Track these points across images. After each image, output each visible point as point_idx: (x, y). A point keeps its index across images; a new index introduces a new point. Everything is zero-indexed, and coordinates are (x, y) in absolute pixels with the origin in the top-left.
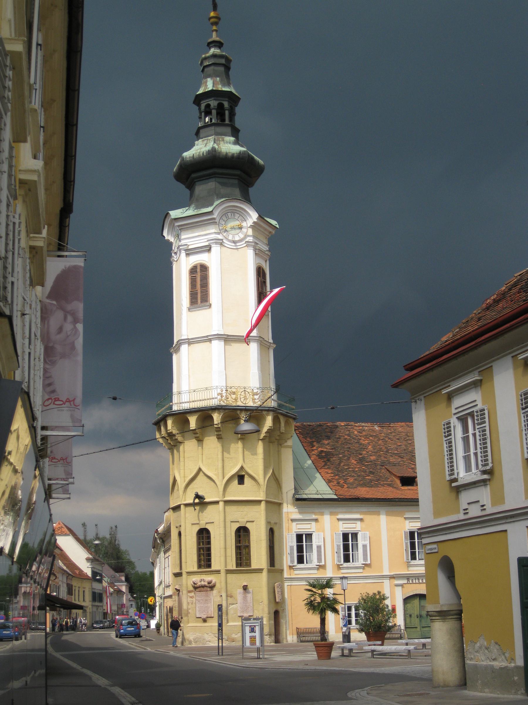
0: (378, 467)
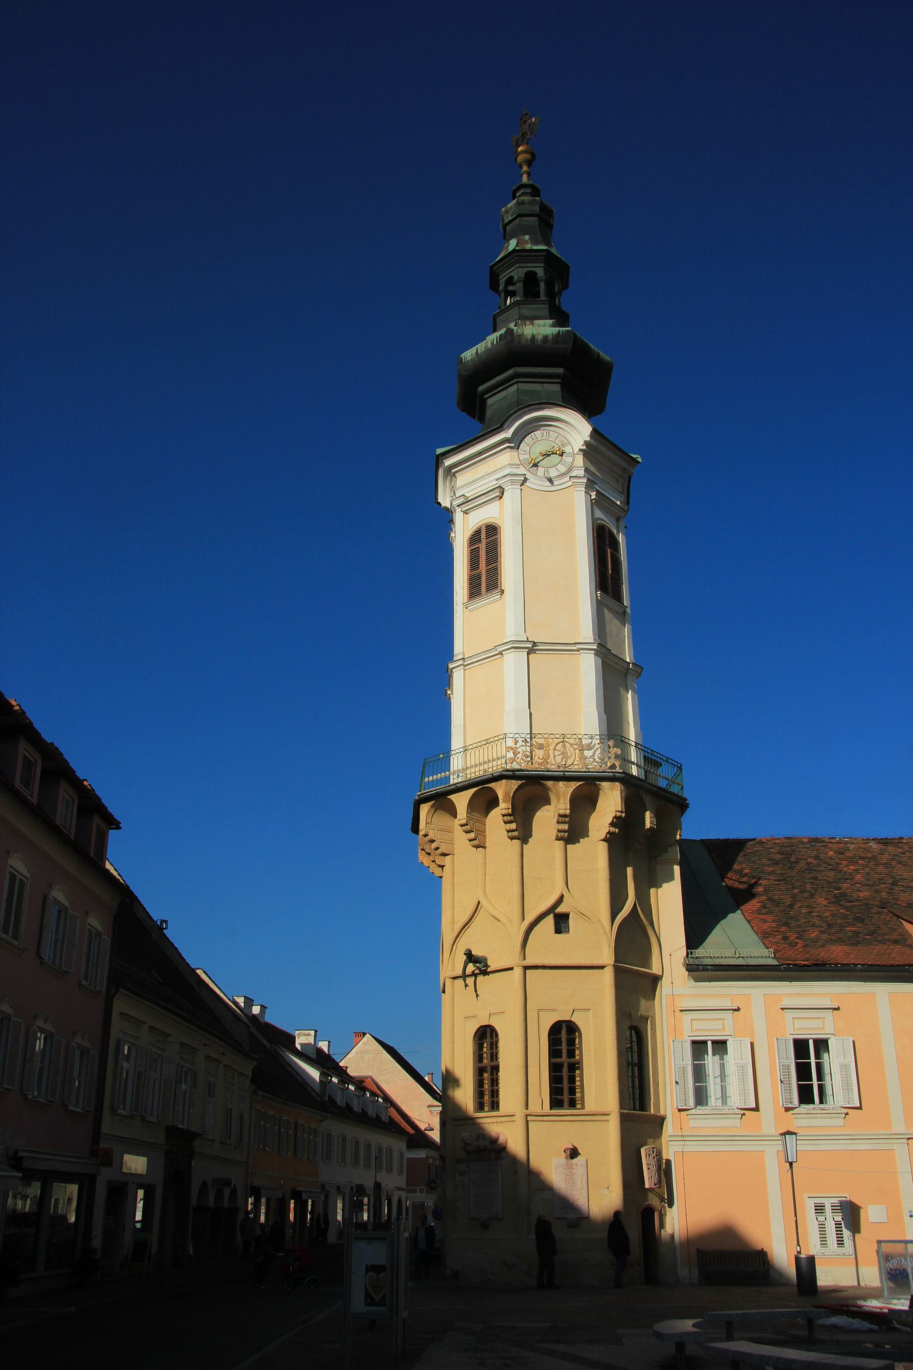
0: (874, 910)
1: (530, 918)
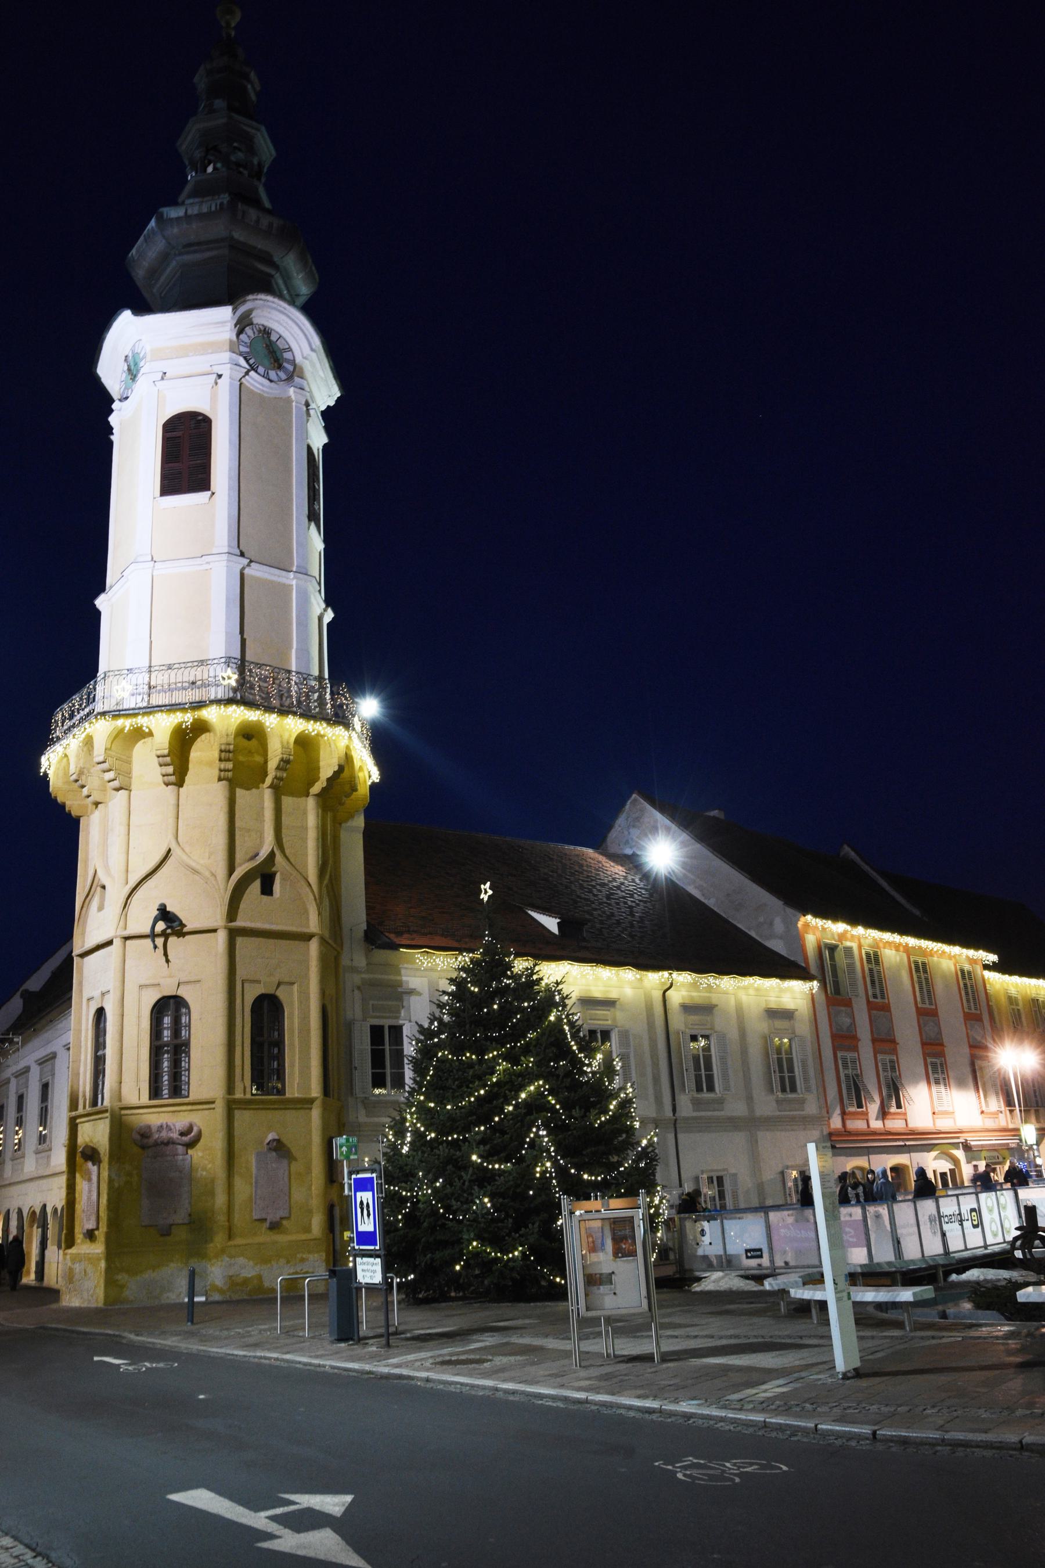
1: (132, 883)
